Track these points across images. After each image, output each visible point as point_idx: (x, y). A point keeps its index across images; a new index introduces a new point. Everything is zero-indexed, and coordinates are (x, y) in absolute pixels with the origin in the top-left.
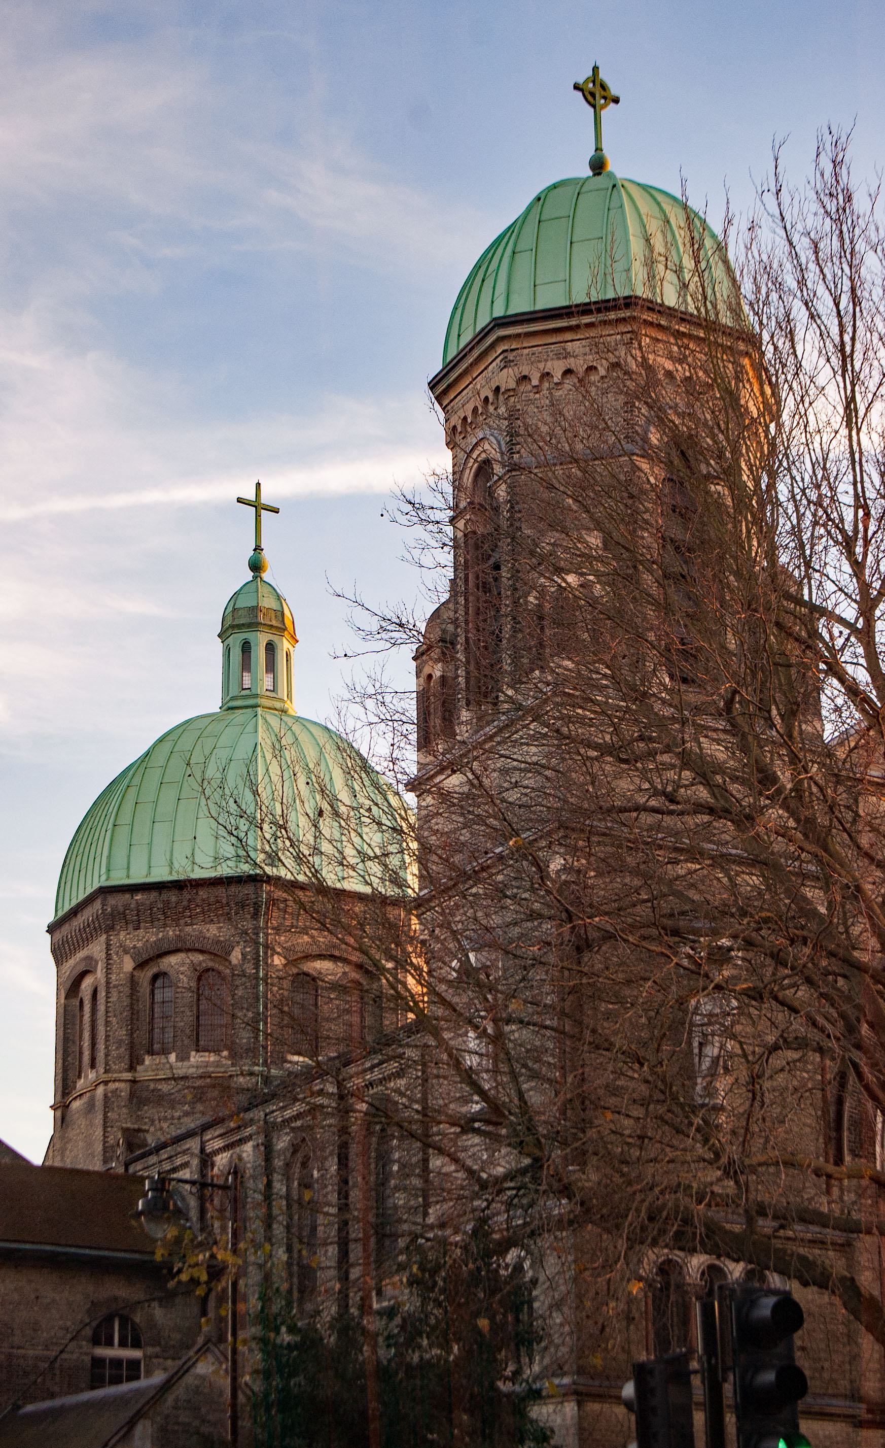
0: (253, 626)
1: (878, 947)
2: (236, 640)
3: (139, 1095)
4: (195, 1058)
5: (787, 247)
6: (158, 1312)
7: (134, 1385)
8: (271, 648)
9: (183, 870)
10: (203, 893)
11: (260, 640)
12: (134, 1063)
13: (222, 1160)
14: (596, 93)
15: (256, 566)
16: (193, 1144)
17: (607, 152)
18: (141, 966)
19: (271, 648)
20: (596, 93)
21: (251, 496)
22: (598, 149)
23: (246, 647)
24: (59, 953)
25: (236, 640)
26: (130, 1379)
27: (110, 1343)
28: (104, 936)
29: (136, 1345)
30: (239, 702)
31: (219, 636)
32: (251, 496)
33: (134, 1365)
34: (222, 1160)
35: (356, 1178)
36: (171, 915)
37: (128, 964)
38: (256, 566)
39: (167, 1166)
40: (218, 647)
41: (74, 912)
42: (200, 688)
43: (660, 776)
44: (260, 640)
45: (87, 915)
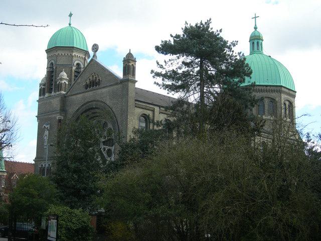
8: (258, 43)
10: (269, 87)
15: (256, 28)
19: (258, 43)
38: (256, 28)
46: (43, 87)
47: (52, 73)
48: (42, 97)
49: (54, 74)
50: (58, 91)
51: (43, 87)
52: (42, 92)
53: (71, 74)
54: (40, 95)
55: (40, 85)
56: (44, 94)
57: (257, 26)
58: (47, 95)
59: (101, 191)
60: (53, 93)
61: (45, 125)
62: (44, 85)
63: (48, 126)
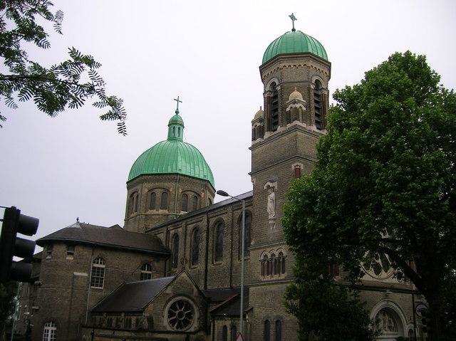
0: (176, 124)
8: (179, 128)
10: (165, 176)
11: (177, 127)
13: (172, 232)
14: (293, 17)
15: (177, 112)
16: (165, 228)
19: (179, 128)
20: (293, 17)
24: (128, 188)
29: (150, 271)
30: (172, 138)
31: (422, 59)
33: (150, 275)
34: (172, 232)
35: (211, 238)
36: (158, 181)
38: (177, 112)
40: (168, 127)
41: (134, 179)
42: (162, 135)
43: (341, 131)
44: (177, 127)
45: (137, 180)
46: (258, 124)
47: (274, 101)
48: (259, 140)
49: (279, 99)
50: (290, 123)
51: (258, 124)
52: (257, 133)
53: (309, 95)
54: (254, 139)
55: (253, 122)
56: (262, 135)
57: (179, 110)
58: (267, 135)
59: (332, 259)
60: (280, 129)
61: (269, 183)
62: (261, 120)
63: (275, 185)
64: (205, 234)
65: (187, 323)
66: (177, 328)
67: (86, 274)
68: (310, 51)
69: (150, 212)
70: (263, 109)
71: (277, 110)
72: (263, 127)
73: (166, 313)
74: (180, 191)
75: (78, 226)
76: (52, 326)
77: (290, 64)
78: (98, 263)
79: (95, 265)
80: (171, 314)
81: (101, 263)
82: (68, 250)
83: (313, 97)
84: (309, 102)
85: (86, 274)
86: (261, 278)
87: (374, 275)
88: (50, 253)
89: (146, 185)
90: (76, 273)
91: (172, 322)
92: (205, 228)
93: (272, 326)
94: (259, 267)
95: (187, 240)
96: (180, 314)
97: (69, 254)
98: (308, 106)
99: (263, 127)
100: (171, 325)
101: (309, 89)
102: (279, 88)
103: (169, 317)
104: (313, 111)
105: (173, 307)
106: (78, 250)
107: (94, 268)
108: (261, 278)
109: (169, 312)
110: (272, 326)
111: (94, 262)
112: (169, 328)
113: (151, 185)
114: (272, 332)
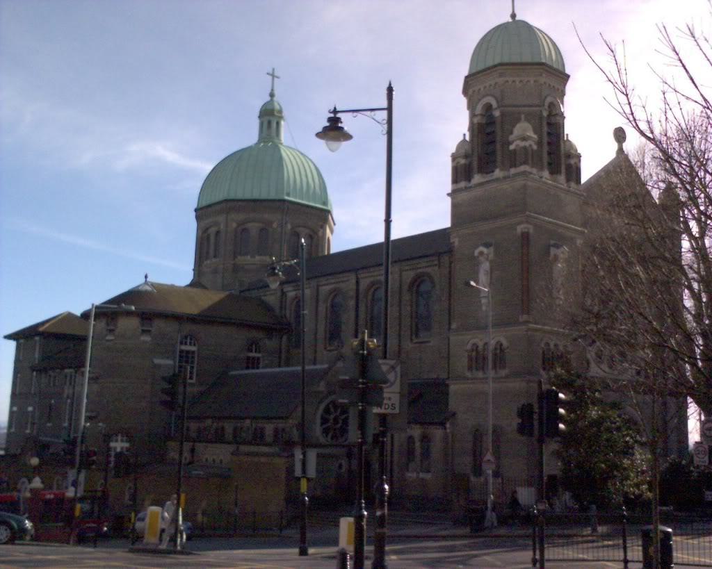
1: (697, 540)
2: (266, 119)
3: (236, 269)
4: (258, 258)
5: (662, 106)
6: (267, 341)
7: (257, 371)
9: (256, 196)
12: (235, 257)
15: (272, 95)
17: (516, 12)
18: (239, 225)
21: (276, 79)
22: (513, 11)
23: (269, 123)
24: (198, 218)
25: (266, 119)
26: (253, 368)
27: (252, 351)
28: (225, 215)
29: (259, 352)
32: (276, 79)
34: (291, 294)
37: (234, 225)
38: (272, 95)
39: (262, 294)
41: (209, 206)
46: (463, 161)
48: (462, 184)
56: (469, 179)
58: (477, 179)
60: (498, 173)
61: (482, 249)
64: (352, 303)
65: (344, 431)
66: (332, 438)
67: (170, 362)
68: (543, 61)
69: (241, 260)
70: (468, 138)
71: (493, 142)
72: (470, 164)
73: (318, 421)
74: (289, 226)
75: (148, 288)
76: (122, 441)
77: (515, 79)
78: (186, 344)
79: (184, 347)
80: (324, 421)
81: (190, 344)
82: (143, 325)
83: (545, 129)
84: (540, 137)
85: (170, 362)
86: (469, 374)
87: (607, 369)
88: (111, 331)
89: (233, 216)
90: (157, 361)
91: (326, 432)
92: (352, 293)
93: (489, 440)
94: (465, 360)
95: (320, 309)
96: (336, 420)
97: (144, 331)
98: (540, 143)
99: (470, 164)
100: (324, 435)
101: (541, 117)
102: (497, 113)
103: (322, 424)
104: (546, 149)
105: (327, 411)
106: (159, 325)
107: (181, 351)
108: (469, 374)
109: (322, 418)
110: (489, 440)
111: (181, 343)
112: (322, 440)
113: (241, 217)
114: (68, 378)
